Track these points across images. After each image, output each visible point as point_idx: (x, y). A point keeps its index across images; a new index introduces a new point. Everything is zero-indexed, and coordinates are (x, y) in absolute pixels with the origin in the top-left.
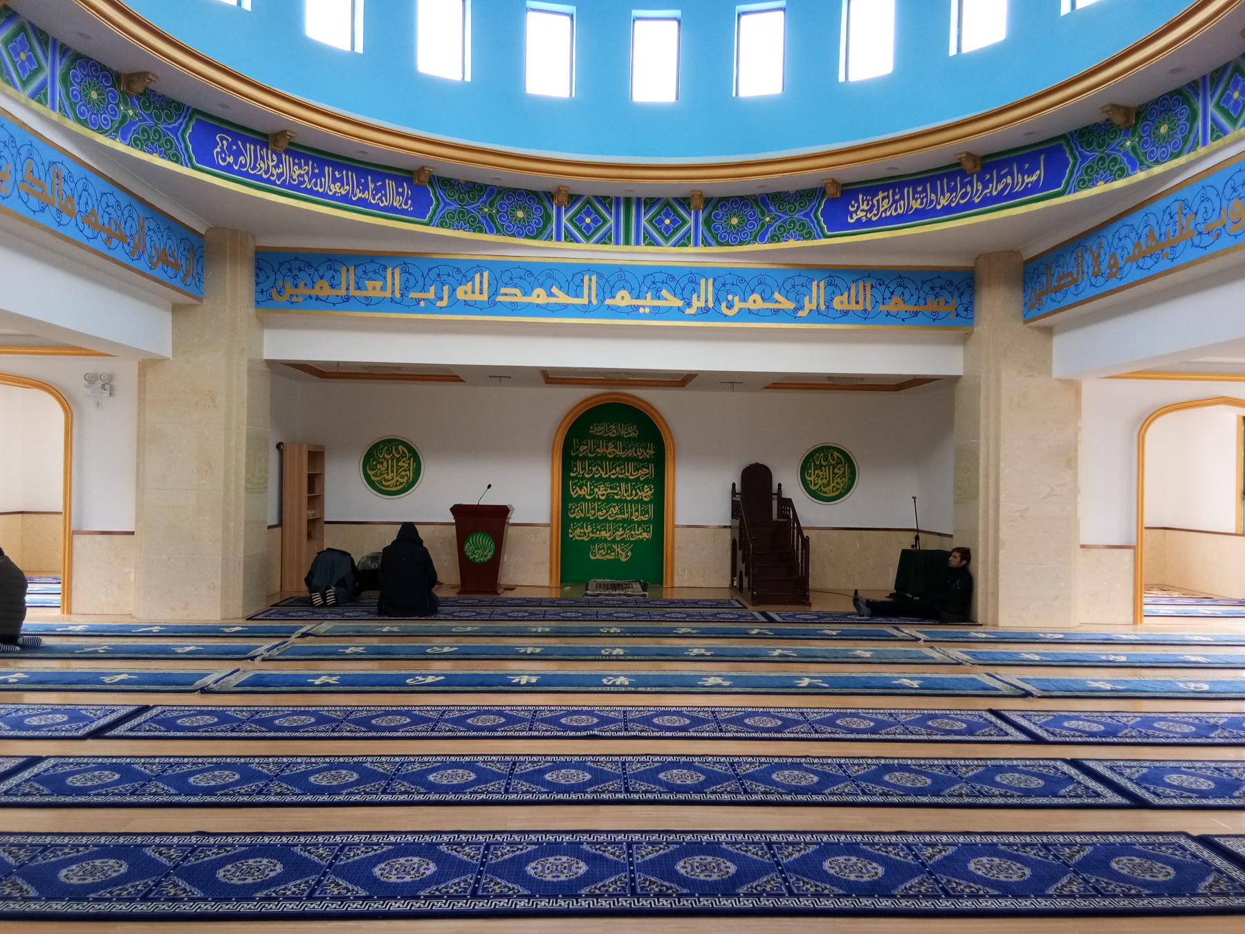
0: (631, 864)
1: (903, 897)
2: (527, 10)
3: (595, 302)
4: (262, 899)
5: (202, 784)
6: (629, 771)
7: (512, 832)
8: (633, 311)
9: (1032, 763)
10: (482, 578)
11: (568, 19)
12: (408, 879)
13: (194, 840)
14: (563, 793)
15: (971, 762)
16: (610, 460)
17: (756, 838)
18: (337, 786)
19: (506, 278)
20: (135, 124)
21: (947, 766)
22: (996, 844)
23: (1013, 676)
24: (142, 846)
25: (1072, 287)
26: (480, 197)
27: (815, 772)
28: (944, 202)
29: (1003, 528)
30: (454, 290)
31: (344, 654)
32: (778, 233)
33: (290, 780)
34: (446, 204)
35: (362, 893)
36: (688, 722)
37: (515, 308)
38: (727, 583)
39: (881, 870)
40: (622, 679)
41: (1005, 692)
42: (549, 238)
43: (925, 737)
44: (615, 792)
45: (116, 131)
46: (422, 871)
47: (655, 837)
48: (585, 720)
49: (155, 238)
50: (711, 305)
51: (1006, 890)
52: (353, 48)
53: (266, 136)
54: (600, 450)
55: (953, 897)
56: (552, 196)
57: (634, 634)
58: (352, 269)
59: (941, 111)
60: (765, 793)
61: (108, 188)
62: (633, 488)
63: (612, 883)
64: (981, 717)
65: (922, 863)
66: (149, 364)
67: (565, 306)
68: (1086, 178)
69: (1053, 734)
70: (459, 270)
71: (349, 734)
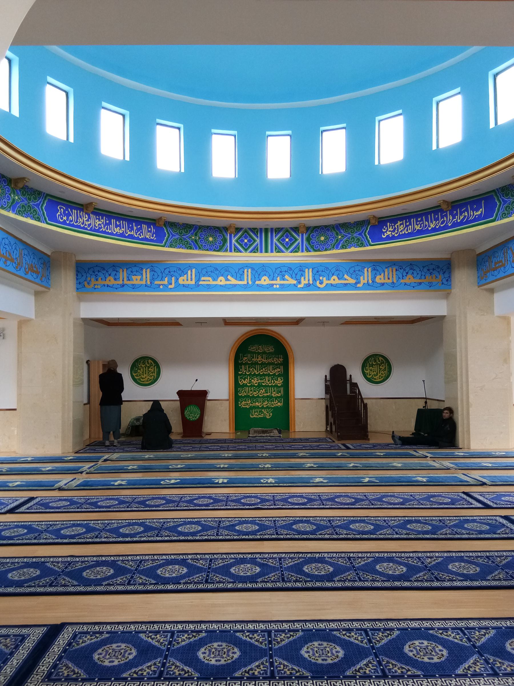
0: (281, 567)
1: (415, 581)
2: (212, 134)
3: (250, 283)
4: (106, 585)
5: (68, 534)
6: (278, 525)
7: (222, 554)
8: (270, 287)
9: (484, 518)
10: (194, 429)
11: (233, 137)
12: (174, 575)
13: (69, 559)
14: (246, 535)
15: (452, 518)
16: (260, 364)
17: (343, 555)
18: (134, 533)
19: (204, 272)
20: (18, 203)
21: (440, 520)
22: (463, 557)
23: (477, 475)
24: (44, 562)
25: (502, 268)
26: (190, 231)
27: (372, 524)
28: (432, 226)
29: (471, 397)
30: (178, 279)
31: (127, 469)
32: (345, 244)
33: (110, 531)
34: (173, 235)
35: (153, 582)
36: (306, 500)
37: (209, 287)
38: (323, 429)
39: (405, 569)
40: (271, 480)
41: (472, 483)
42: (226, 251)
43: (429, 506)
44: (271, 535)
45: (10, 208)
46: (180, 571)
47: (292, 555)
48: (254, 501)
49: (27, 259)
50: (311, 282)
51: (466, 577)
52: (124, 158)
53: (82, 205)
54: (254, 360)
55: (440, 581)
56: (227, 229)
57: (276, 456)
58: (125, 270)
59: (429, 180)
60: (347, 534)
61: (5, 235)
62: (272, 379)
63: (272, 576)
64: (458, 496)
65: (426, 566)
66: (23, 322)
67: (235, 285)
68: (506, 212)
69: (496, 504)
70: (180, 269)
71: (136, 509)
